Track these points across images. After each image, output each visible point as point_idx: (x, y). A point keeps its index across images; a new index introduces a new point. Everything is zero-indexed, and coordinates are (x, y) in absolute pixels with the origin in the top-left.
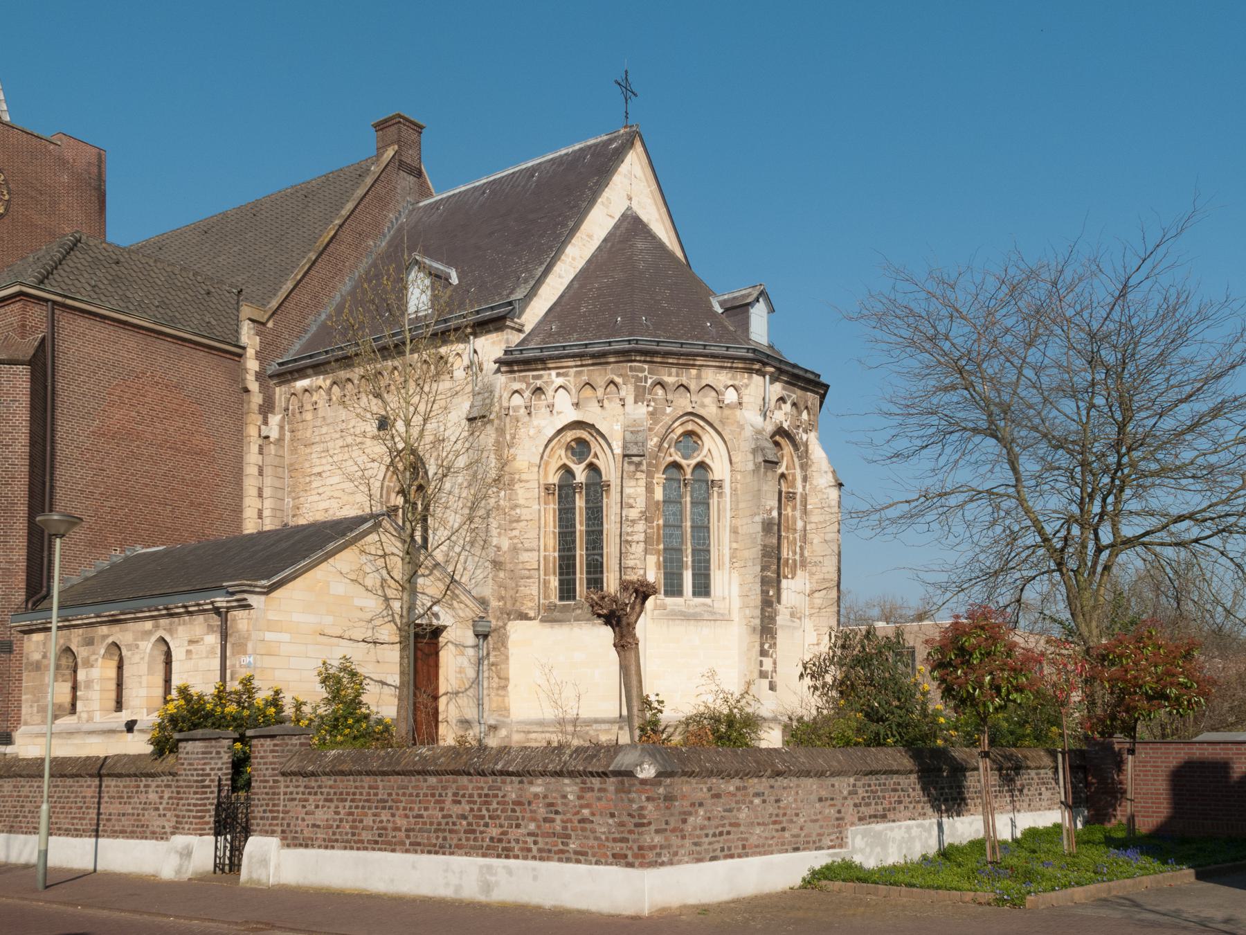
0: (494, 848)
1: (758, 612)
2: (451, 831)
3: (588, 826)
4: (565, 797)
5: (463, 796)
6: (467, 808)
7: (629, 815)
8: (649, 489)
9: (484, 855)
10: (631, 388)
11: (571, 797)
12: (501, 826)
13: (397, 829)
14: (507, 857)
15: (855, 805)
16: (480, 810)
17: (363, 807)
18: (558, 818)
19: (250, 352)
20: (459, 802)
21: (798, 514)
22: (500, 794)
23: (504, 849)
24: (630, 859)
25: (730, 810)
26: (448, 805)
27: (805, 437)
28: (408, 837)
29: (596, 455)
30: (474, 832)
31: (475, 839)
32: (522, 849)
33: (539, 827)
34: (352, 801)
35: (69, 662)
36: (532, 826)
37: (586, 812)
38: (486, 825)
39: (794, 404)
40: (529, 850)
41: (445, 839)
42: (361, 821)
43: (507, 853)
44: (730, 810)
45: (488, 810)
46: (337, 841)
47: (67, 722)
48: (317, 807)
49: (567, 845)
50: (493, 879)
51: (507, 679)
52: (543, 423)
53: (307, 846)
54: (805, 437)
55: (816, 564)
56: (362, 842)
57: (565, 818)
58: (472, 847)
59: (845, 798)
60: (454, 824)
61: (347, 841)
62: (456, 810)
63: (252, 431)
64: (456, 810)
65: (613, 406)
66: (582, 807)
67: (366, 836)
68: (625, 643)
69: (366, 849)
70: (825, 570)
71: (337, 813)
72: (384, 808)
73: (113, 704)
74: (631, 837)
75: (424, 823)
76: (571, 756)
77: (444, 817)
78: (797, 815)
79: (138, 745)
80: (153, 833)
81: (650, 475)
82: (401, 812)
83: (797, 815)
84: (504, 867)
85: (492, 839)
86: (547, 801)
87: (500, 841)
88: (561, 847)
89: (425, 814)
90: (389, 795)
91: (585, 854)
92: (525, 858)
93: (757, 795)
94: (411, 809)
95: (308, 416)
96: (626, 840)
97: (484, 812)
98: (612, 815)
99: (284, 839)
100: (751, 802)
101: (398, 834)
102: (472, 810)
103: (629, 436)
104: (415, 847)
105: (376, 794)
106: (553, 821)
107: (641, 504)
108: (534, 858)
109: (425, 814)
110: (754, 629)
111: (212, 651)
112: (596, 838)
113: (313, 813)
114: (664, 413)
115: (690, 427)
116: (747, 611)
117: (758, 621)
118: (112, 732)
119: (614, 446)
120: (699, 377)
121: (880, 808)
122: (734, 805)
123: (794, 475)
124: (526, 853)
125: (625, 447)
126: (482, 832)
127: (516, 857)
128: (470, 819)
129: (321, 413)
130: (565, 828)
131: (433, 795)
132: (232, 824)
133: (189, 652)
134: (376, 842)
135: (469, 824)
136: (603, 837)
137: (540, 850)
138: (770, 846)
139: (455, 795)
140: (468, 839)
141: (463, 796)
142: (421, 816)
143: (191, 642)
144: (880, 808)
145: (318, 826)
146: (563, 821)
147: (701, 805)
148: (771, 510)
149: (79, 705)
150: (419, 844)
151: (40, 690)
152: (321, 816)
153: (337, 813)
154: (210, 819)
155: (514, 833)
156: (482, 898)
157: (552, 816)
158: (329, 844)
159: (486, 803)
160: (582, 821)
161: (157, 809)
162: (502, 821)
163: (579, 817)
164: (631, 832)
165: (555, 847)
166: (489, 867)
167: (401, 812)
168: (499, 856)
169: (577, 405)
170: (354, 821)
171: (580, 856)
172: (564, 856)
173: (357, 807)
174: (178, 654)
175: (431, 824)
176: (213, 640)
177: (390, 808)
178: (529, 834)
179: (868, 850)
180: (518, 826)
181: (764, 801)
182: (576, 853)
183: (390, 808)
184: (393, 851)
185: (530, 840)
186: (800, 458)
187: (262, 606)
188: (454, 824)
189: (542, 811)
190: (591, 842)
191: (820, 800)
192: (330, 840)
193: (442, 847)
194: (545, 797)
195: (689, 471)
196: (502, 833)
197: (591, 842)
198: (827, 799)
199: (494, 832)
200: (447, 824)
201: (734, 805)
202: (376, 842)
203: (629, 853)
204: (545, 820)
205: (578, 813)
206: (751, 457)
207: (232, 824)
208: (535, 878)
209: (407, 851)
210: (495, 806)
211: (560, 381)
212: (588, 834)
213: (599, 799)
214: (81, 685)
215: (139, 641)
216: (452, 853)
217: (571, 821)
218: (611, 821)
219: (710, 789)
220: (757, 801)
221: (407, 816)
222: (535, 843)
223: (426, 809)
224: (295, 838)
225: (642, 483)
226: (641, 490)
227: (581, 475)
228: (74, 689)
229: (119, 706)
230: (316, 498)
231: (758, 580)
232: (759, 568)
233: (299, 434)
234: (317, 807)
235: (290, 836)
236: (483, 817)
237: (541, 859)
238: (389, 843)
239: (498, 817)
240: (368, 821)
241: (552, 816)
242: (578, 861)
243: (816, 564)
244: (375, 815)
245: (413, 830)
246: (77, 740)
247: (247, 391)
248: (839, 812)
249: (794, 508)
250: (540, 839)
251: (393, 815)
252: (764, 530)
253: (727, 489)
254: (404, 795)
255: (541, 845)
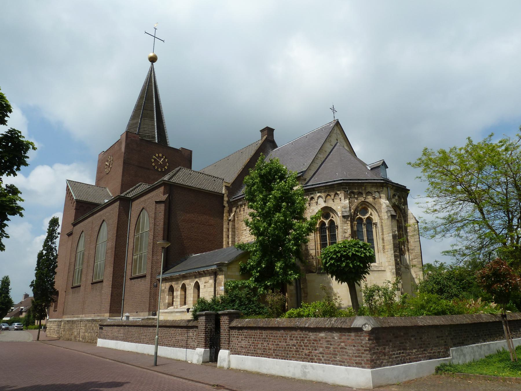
0: (307, 358)
1: (394, 267)
2: (290, 351)
3: (344, 350)
4: (334, 338)
5: (294, 337)
6: (295, 342)
7: (361, 346)
8: (352, 227)
9: (303, 361)
10: (343, 194)
11: (336, 338)
12: (309, 350)
13: (270, 349)
14: (312, 362)
15: (451, 339)
16: (300, 343)
17: (258, 341)
18: (332, 347)
19: (225, 195)
20: (292, 340)
21: (404, 233)
22: (308, 337)
23: (311, 359)
24: (363, 365)
25: (402, 343)
26: (288, 341)
27: (403, 207)
28: (274, 352)
29: (332, 217)
30: (298, 351)
31: (299, 355)
32: (317, 359)
33: (324, 350)
34: (254, 338)
35: (171, 290)
36: (321, 349)
37: (343, 344)
38: (303, 349)
39: (399, 197)
40: (321, 360)
41: (288, 354)
42: (257, 346)
43: (312, 360)
44: (402, 343)
45: (303, 343)
46: (249, 353)
47: (171, 309)
48: (242, 340)
49: (336, 358)
50: (307, 371)
51: (307, 293)
52: (314, 208)
53: (239, 354)
54: (403, 207)
55: (412, 250)
56: (258, 354)
57: (334, 346)
58: (298, 358)
59: (447, 336)
60: (291, 348)
61: (252, 353)
62: (291, 343)
63: (225, 218)
64: (291, 343)
65: (337, 201)
66: (341, 342)
67: (259, 351)
68: (156, 353)
69: (259, 356)
70: (416, 251)
71: (249, 342)
72: (265, 341)
73: (183, 303)
74: (363, 355)
75: (280, 347)
76: (335, 321)
77: (287, 345)
78: (429, 344)
79: (189, 316)
80: (191, 347)
81: (352, 222)
82: (271, 343)
83: (429, 344)
84: (311, 366)
85: (306, 354)
86: (326, 340)
87: (309, 355)
88: (333, 359)
89: (280, 344)
90: (267, 336)
91: (344, 362)
92: (319, 363)
93: (412, 336)
94: (275, 342)
95: (242, 212)
96: (361, 357)
97: (302, 344)
98: (354, 346)
99: (231, 351)
100: (410, 339)
101: (270, 351)
102: (297, 343)
103: (343, 210)
104: (277, 357)
105: (262, 336)
106: (329, 348)
107: (349, 231)
108: (323, 363)
109: (280, 344)
110: (393, 273)
111: (211, 285)
112: (348, 356)
113: (240, 342)
114: (355, 202)
115: (364, 206)
116: (390, 267)
117: (395, 270)
118: (183, 312)
119: (339, 214)
120: (365, 189)
121: (461, 340)
122: (403, 341)
123: (401, 220)
124: (319, 361)
125: (342, 213)
126: (301, 352)
127: (316, 362)
128: (297, 347)
129: (245, 211)
130: (334, 351)
131: (282, 337)
132: (213, 344)
133: (205, 286)
134: (263, 354)
135: (297, 348)
136: (351, 355)
137: (325, 360)
138: (420, 357)
139: (290, 337)
140: (296, 354)
141: (294, 337)
142: (278, 345)
143: (205, 282)
144: (461, 340)
145: (243, 347)
146: (333, 348)
147: (390, 341)
148: (395, 231)
149: (174, 303)
150: (278, 355)
151: (164, 298)
152: (243, 343)
153: (249, 342)
154: (367, 356)
155: (315, 352)
156: (303, 378)
157: (329, 346)
158: (247, 354)
159: (302, 340)
160: (341, 348)
161: (192, 339)
162: (309, 348)
163: (340, 346)
164: (362, 353)
165: (331, 359)
166: (305, 366)
167: (271, 343)
168: (309, 362)
169: (325, 202)
170: (255, 346)
171: (341, 363)
172: (335, 363)
173: (255, 340)
174: (202, 286)
175: (282, 348)
176: (211, 281)
177: (267, 341)
178: (320, 353)
179: (458, 357)
180: (316, 350)
181: (415, 339)
182: (340, 361)
183: (267, 341)
184: (269, 358)
185: (320, 355)
186: (402, 214)
187: (226, 270)
188: (291, 348)
189: (325, 345)
190: (346, 357)
191: (438, 337)
192: (247, 353)
193: (287, 357)
194: (326, 338)
195: (365, 220)
196: (309, 353)
197: (346, 357)
198: (440, 337)
199: (307, 352)
200: (288, 348)
201: (403, 341)
202: (263, 354)
203: (363, 362)
204: (326, 347)
205: (339, 345)
206: (386, 214)
207: (213, 344)
208: (324, 371)
209: (274, 358)
210: (306, 341)
211: (319, 194)
212: (344, 353)
213: (348, 339)
214: (175, 297)
215: (190, 284)
216: (291, 360)
217: (336, 348)
218: (354, 348)
219: (393, 334)
220: (412, 339)
221: (273, 345)
222: (323, 357)
223: (280, 342)
224: (235, 351)
225: (349, 224)
226: (349, 227)
227: (327, 222)
228: (173, 298)
229: (185, 304)
230: (245, 237)
231: (393, 256)
232: (393, 252)
233: (239, 218)
234: (242, 340)
235: (233, 350)
236: (301, 346)
237: (326, 363)
238: (267, 355)
239: (308, 346)
240: (260, 346)
241: (329, 346)
242: (341, 365)
243: (412, 250)
244: (262, 344)
245: (276, 350)
246: (173, 314)
247: (224, 207)
248: (445, 342)
249: (402, 231)
250: (324, 355)
251: (268, 344)
252: (393, 238)
253: (379, 225)
254: (272, 336)
255: (325, 358)
